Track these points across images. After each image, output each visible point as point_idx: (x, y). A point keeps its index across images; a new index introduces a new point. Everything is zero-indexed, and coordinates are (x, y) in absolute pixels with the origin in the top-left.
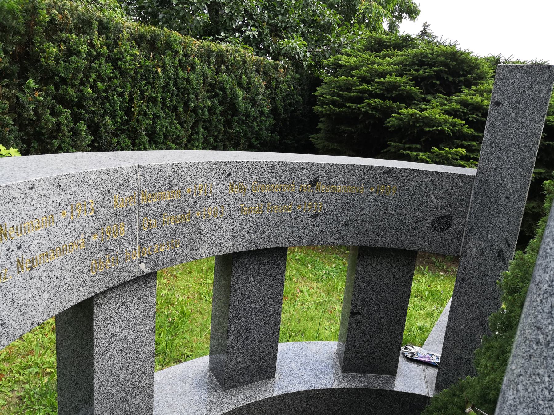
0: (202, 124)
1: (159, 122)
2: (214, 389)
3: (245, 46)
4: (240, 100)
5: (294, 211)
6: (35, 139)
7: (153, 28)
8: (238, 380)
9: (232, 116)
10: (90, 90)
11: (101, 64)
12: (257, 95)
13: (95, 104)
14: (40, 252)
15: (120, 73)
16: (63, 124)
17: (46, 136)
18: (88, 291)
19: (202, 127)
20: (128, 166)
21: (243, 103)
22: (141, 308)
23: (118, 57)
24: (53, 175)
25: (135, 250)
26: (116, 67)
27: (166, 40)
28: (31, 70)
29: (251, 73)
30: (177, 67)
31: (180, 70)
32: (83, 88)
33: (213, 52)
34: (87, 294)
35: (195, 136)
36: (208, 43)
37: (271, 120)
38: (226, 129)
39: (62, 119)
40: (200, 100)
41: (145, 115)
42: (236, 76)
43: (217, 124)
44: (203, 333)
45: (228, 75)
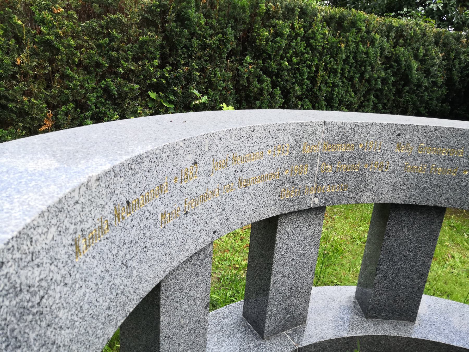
0: (373, 92)
1: (336, 90)
2: (357, 314)
3: (427, 19)
4: (414, 71)
5: (459, 175)
6: (245, 100)
7: (343, 9)
8: (380, 313)
9: (404, 86)
10: (287, 63)
11: (297, 43)
12: (432, 66)
13: (289, 74)
14: (252, 176)
15: (311, 50)
16: (264, 89)
17: (252, 98)
18: (277, 210)
19: (374, 95)
20: (317, 121)
21: (417, 74)
22: (310, 232)
23: (311, 36)
24: (267, 124)
25: (313, 187)
26: (309, 44)
27: (352, 20)
28: (249, 49)
29: (430, 45)
30: (358, 42)
31: (361, 45)
32: (282, 61)
33: (394, 27)
34: (276, 212)
35: (366, 103)
36: (390, 19)
37: (444, 91)
38: (395, 97)
39: (265, 85)
40: (375, 72)
41: (326, 83)
42: (412, 49)
43: (388, 93)
44: (352, 270)
45: (406, 48)
